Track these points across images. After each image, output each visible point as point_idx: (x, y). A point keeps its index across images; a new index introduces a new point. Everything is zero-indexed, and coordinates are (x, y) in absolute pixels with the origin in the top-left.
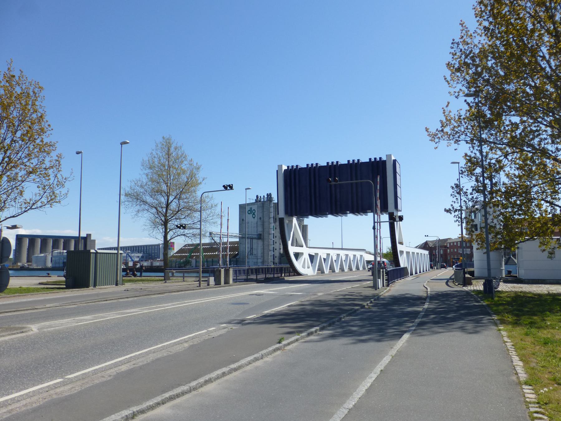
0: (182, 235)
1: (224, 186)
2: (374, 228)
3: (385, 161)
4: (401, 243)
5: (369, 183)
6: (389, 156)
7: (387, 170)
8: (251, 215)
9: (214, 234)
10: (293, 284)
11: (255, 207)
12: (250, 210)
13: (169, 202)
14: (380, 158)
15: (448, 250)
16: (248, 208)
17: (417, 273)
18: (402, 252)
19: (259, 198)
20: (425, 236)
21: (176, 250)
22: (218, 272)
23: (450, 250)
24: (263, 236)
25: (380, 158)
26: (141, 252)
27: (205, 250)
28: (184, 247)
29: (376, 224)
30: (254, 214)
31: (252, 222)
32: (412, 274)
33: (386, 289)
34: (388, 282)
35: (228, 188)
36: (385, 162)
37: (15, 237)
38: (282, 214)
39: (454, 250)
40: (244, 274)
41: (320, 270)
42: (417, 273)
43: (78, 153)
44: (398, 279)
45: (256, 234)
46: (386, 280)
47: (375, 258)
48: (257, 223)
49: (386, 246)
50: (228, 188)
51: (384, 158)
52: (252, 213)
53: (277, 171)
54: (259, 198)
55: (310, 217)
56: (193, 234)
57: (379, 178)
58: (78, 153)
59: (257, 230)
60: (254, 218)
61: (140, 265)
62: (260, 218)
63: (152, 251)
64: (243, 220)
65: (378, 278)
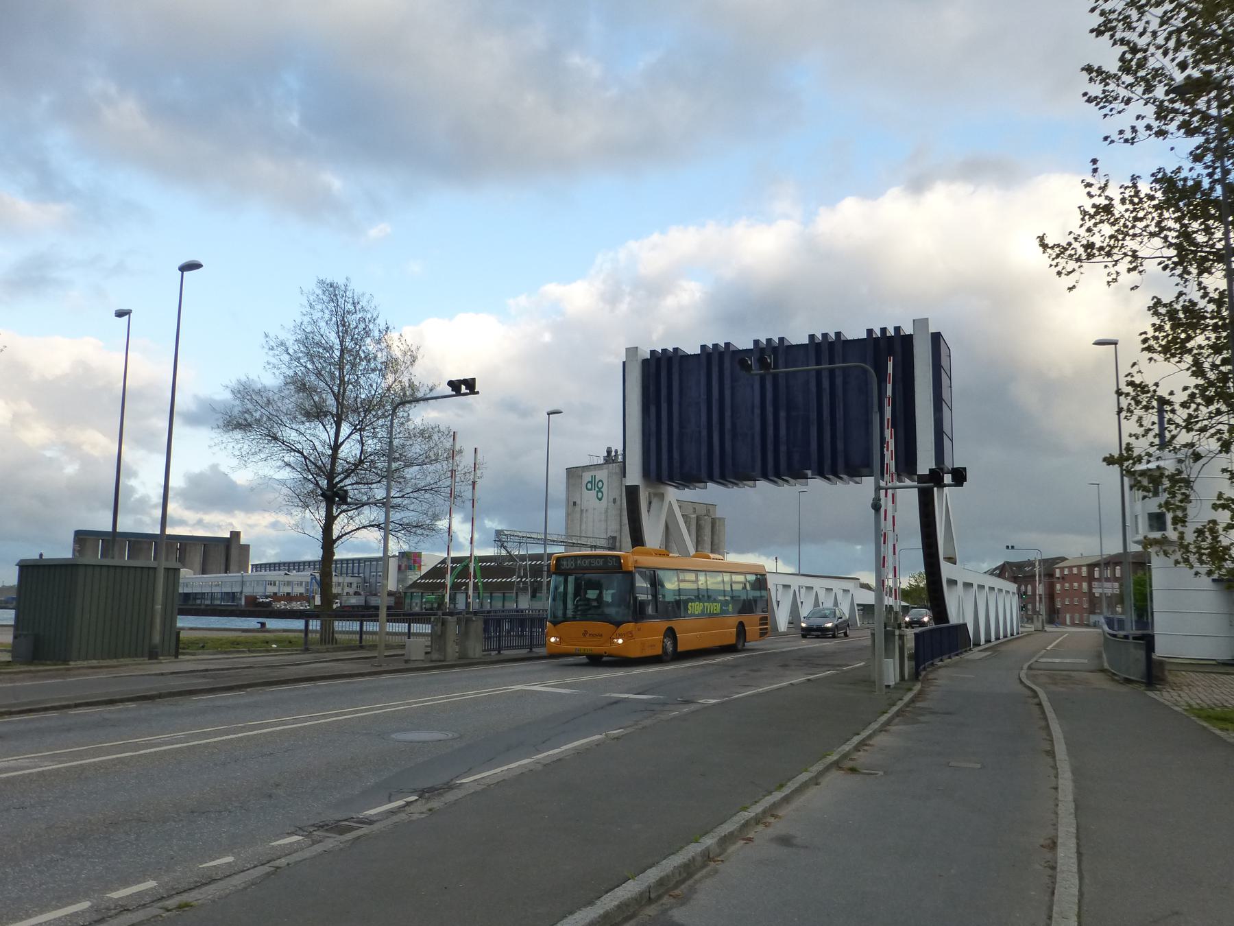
0: (373, 526)
1: (451, 383)
2: (876, 507)
3: (911, 337)
4: (952, 560)
5: (865, 371)
6: (921, 323)
7: (918, 452)
8: (594, 492)
9: (505, 535)
10: (617, 669)
11: (601, 475)
12: (591, 482)
13: (340, 440)
14: (897, 329)
15: (1058, 586)
16: (587, 477)
17: (990, 641)
18: (953, 582)
19: (613, 453)
20: (1008, 547)
21: (424, 570)
22: (440, 624)
23: (1063, 586)
24: (620, 541)
25: (897, 329)
26: (347, 574)
27: (486, 572)
28: (439, 563)
29: (883, 492)
30: (600, 490)
31: (594, 509)
32: (977, 644)
33: (910, 690)
34: (917, 666)
35: (463, 389)
36: (909, 338)
37: (72, 536)
38: (634, 477)
39: (1071, 586)
40: (336, 640)
41: (792, 623)
42: (990, 641)
43: (120, 314)
44: (944, 657)
45: (604, 536)
46: (910, 658)
47: (879, 598)
48: (606, 512)
49: (910, 576)
50: (463, 389)
51: (908, 330)
52: (596, 489)
53: (624, 363)
54: (613, 453)
55: (710, 485)
56: (401, 525)
57: (890, 365)
58: (120, 314)
59: (607, 529)
60: (600, 499)
61: (341, 603)
62: (615, 501)
63: (371, 572)
64: (575, 503)
65: (887, 657)
